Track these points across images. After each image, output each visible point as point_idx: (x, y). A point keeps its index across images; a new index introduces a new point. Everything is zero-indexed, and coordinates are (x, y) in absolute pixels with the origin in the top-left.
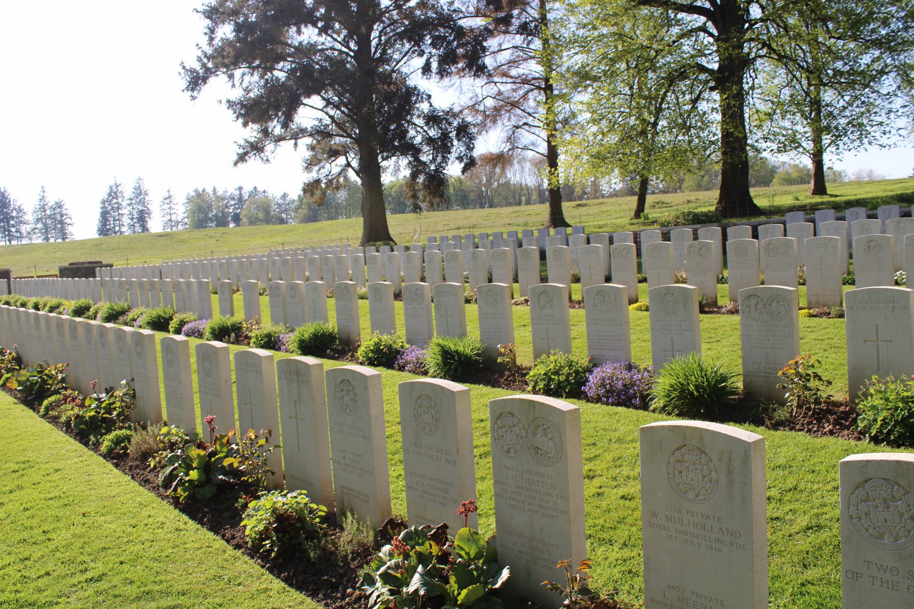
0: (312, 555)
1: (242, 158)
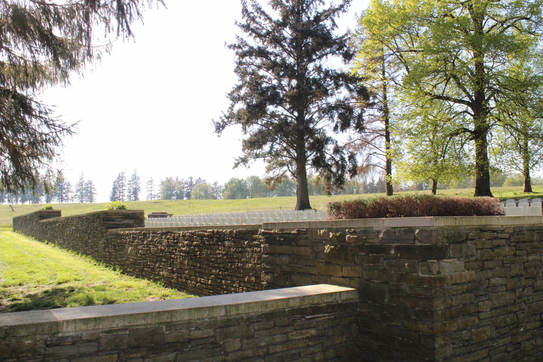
1: (236, 165)
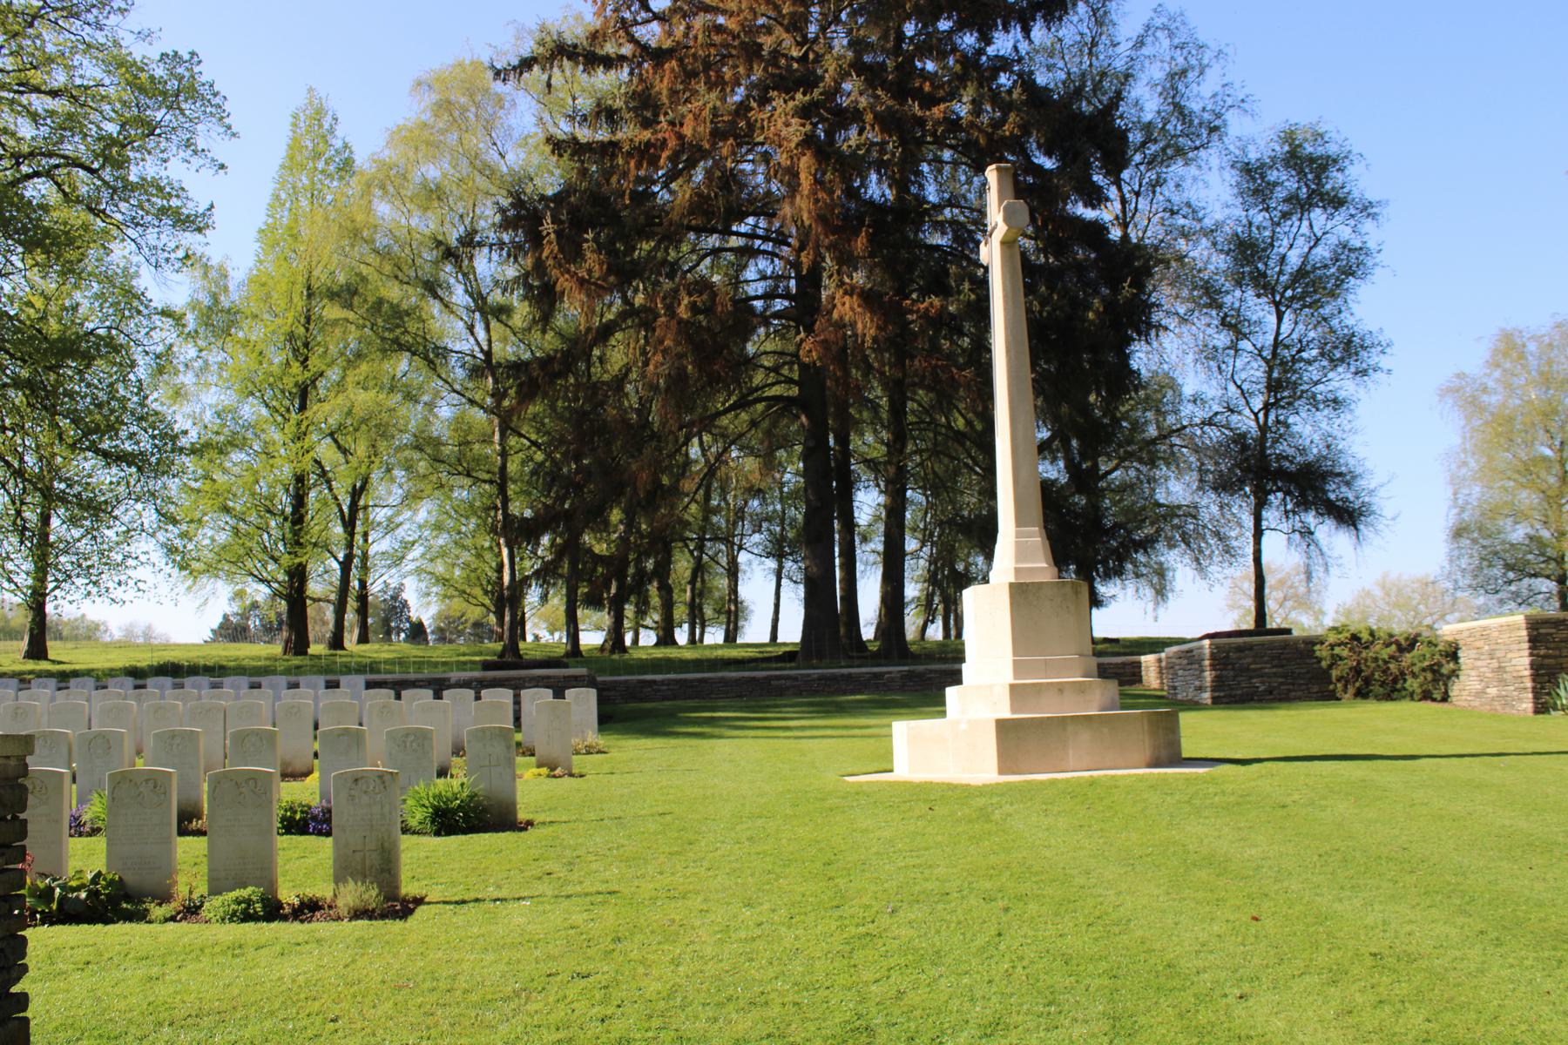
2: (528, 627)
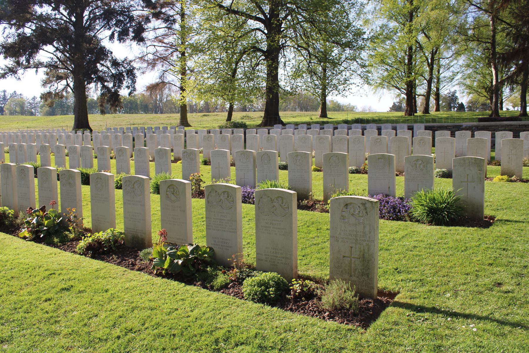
0: (7, 222)
2: (504, 105)
